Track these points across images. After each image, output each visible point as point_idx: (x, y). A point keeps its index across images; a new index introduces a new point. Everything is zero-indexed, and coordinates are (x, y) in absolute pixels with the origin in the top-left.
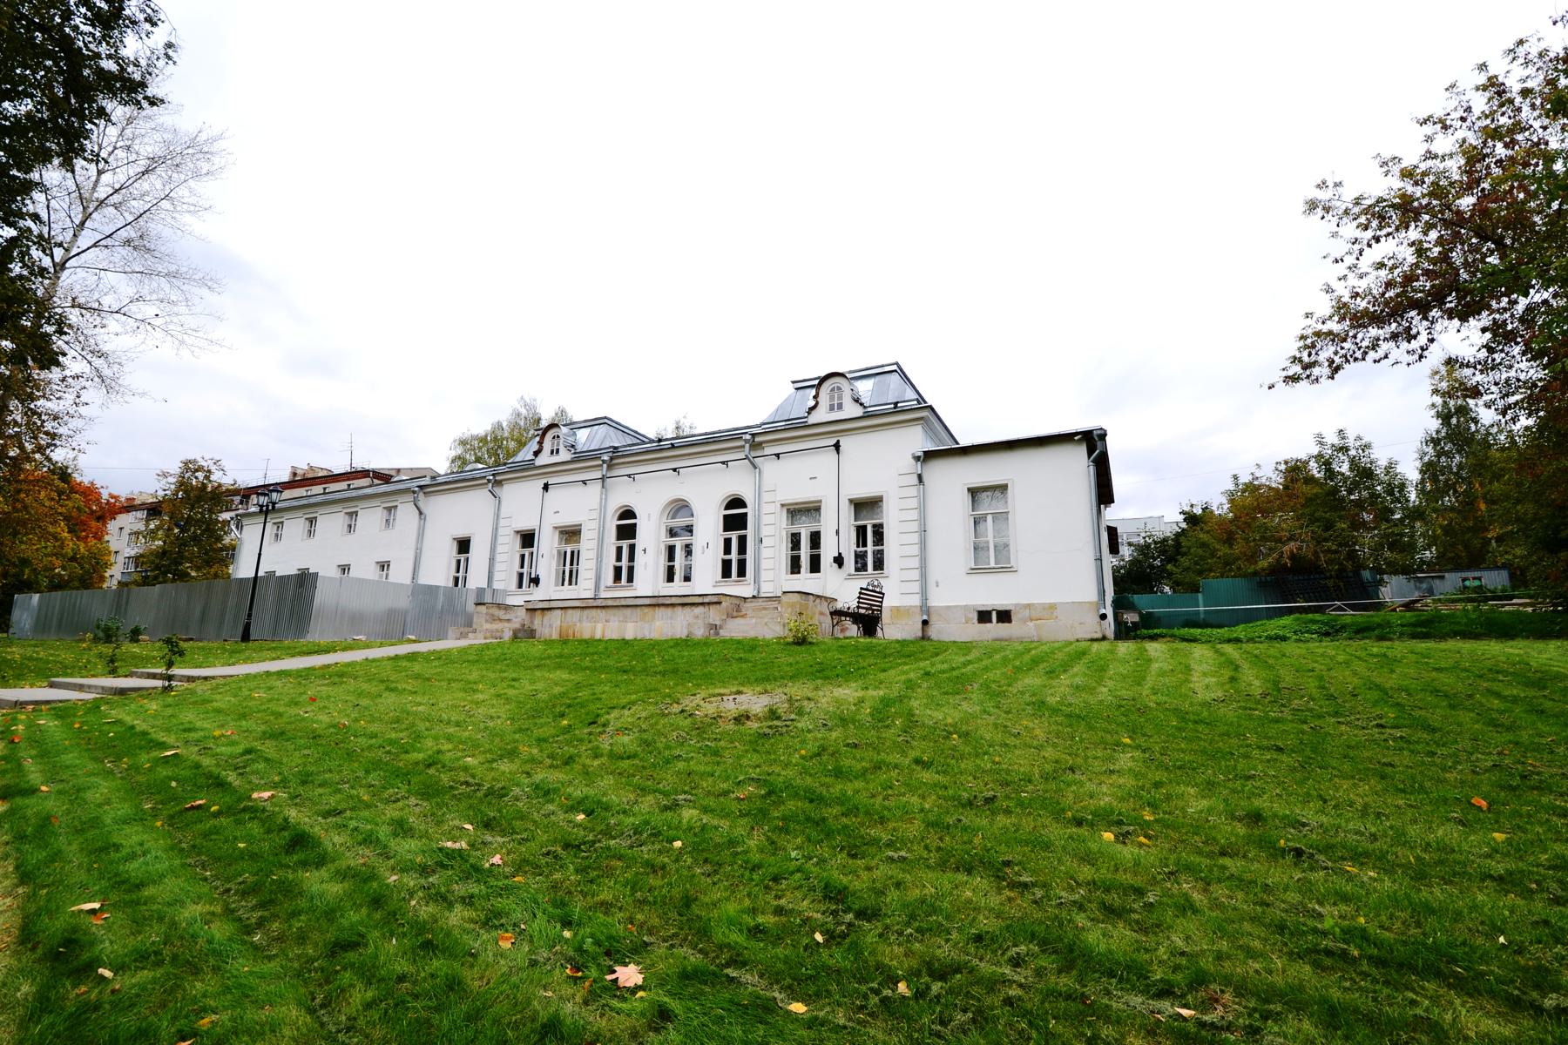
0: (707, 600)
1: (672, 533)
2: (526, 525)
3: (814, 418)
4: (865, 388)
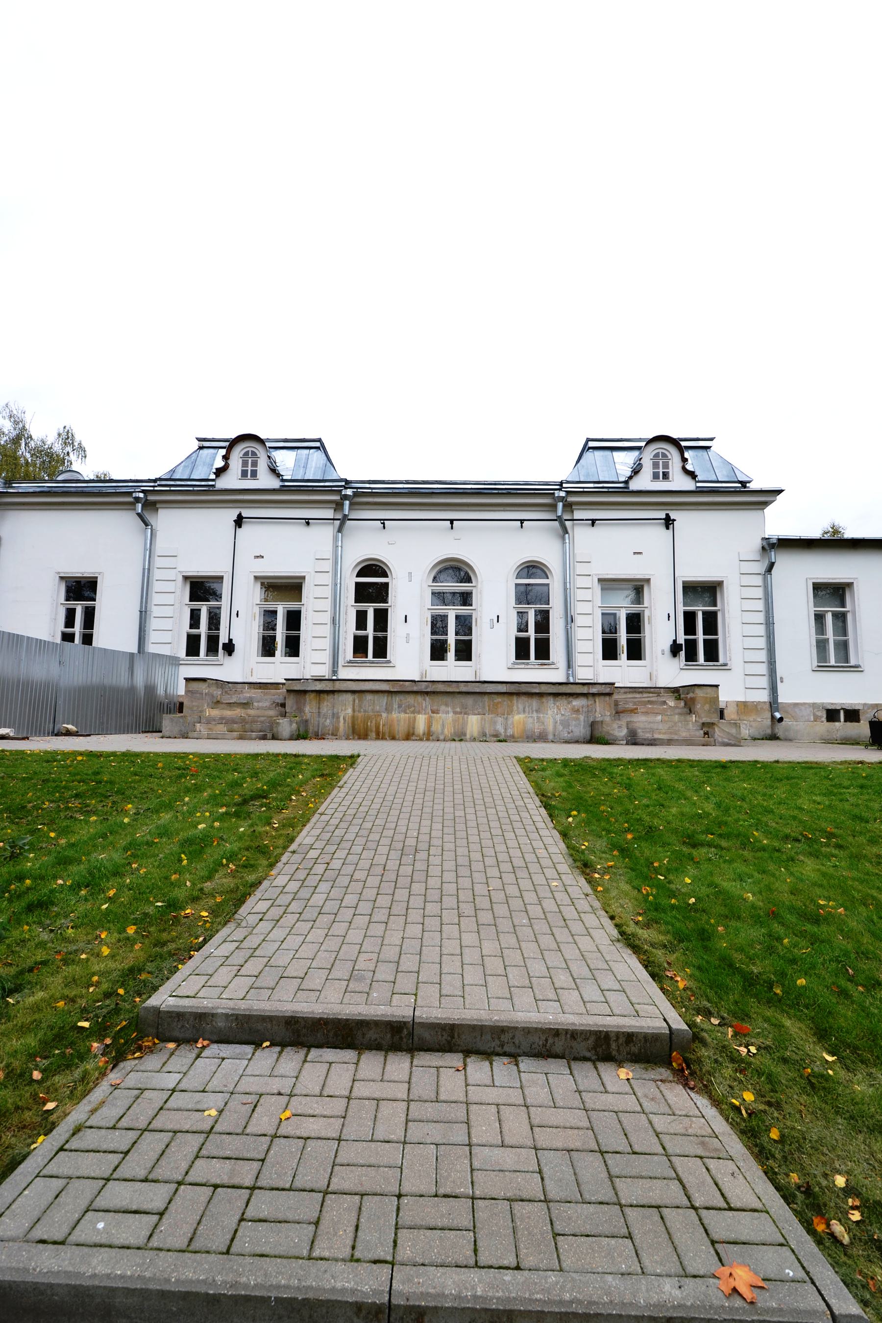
0: (594, 690)
1: (439, 597)
2: (202, 568)
3: (223, 483)
4: (286, 461)
